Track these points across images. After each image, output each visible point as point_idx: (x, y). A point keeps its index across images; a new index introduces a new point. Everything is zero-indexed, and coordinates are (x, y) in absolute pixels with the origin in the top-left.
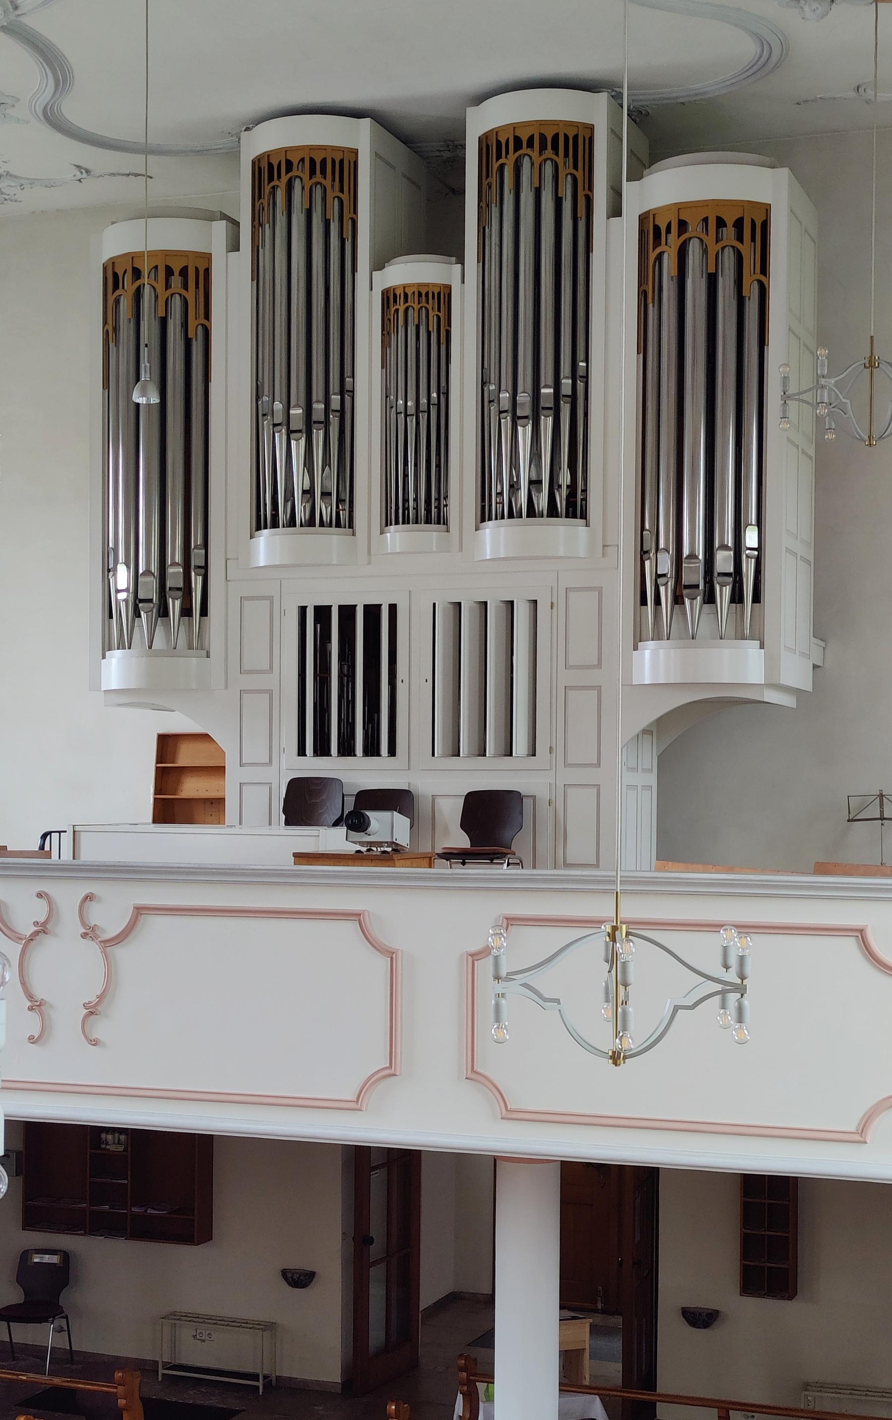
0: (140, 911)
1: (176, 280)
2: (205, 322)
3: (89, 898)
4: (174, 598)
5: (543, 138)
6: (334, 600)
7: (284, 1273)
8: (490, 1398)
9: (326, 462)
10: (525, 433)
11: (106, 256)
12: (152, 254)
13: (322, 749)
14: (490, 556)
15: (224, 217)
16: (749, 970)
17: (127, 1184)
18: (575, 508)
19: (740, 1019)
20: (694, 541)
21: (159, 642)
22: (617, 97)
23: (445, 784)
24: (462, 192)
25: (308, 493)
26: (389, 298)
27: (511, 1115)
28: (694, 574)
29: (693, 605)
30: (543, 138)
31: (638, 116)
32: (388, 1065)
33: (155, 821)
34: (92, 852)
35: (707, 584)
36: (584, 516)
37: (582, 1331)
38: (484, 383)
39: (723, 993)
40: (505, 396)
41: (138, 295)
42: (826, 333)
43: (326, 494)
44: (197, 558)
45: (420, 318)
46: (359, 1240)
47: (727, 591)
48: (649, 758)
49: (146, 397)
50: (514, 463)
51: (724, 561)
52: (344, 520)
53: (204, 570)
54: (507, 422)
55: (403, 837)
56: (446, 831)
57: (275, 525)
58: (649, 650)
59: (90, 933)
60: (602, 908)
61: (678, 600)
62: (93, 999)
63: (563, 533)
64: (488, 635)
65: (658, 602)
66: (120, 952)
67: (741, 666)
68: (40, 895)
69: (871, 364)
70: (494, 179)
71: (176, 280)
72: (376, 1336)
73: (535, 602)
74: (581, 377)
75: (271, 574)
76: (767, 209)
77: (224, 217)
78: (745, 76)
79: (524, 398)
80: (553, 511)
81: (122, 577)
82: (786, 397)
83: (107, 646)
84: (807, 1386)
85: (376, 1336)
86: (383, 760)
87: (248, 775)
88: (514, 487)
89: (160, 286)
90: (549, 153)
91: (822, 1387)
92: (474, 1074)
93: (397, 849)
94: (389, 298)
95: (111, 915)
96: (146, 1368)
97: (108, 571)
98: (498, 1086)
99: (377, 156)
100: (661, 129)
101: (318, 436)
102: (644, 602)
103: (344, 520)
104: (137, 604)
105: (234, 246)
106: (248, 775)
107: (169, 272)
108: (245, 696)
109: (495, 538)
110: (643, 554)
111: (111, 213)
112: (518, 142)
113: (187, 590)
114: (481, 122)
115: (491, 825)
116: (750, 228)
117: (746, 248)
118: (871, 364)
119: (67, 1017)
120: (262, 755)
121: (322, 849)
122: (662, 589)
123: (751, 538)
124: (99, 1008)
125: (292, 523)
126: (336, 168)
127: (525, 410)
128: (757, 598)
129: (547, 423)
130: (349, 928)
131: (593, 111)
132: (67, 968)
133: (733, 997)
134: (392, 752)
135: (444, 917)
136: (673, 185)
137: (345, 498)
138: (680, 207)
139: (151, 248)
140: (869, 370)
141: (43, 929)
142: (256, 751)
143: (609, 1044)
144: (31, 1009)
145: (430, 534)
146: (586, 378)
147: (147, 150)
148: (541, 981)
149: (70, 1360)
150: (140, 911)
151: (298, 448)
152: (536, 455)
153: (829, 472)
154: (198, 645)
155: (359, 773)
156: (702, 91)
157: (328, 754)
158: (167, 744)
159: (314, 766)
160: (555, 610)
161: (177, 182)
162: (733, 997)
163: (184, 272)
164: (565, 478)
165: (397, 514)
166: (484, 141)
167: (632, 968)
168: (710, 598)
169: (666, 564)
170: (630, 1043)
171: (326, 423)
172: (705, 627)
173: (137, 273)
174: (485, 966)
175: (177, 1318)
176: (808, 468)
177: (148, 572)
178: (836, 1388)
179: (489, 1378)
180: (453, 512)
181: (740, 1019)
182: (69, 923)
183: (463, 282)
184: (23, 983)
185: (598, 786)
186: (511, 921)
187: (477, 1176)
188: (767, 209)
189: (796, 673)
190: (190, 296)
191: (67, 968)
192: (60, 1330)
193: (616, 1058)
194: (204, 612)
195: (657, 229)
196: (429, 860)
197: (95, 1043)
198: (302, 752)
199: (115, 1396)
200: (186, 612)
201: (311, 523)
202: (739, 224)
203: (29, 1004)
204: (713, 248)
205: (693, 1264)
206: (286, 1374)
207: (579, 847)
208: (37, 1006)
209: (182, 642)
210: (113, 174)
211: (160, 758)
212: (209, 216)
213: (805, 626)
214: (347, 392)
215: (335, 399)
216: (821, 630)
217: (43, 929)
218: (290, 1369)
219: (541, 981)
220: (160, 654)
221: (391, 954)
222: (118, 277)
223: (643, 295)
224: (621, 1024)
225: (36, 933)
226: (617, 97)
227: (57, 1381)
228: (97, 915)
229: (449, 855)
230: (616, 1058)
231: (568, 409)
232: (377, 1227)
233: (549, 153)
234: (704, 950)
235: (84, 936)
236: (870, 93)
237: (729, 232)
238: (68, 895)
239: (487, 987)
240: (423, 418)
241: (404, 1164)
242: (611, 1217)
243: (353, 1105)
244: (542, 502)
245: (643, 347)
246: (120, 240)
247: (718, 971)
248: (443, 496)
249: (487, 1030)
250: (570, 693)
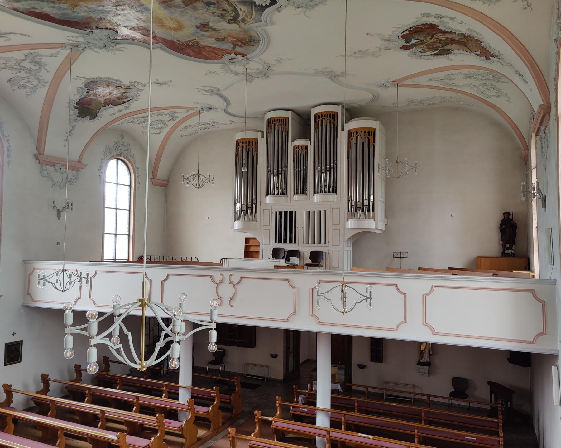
0: (242, 278)
1: (251, 144)
4: (249, 210)
5: (327, 115)
6: (283, 210)
7: (271, 355)
8: (316, 384)
9: (282, 181)
10: (323, 176)
11: (237, 139)
12: (246, 139)
13: (280, 242)
15: (261, 131)
16: (372, 294)
18: (334, 191)
19: (370, 305)
20: (359, 198)
21: (246, 219)
22: (343, 106)
23: (306, 249)
24: (310, 125)
25: (278, 188)
26: (295, 147)
27: (320, 323)
28: (359, 205)
29: (359, 212)
30: (327, 115)
31: (348, 110)
33: (245, 257)
34: (232, 264)
35: (363, 208)
36: (336, 193)
37: (336, 370)
38: (315, 165)
39: (366, 299)
40: (319, 168)
41: (243, 147)
42: (387, 155)
43: (281, 188)
44: (254, 202)
45: (301, 152)
46: (287, 348)
47: (367, 209)
48: (350, 244)
49: (244, 170)
50: (321, 182)
51: (366, 202)
52: (285, 194)
53: (256, 204)
55: (297, 263)
56: (307, 260)
57: (271, 194)
58: (350, 221)
59: (231, 282)
60: (340, 279)
61: (356, 211)
63: (331, 197)
64: (315, 218)
65: (352, 211)
66: (237, 287)
67: (370, 225)
69: (397, 162)
70: (317, 123)
71: (251, 144)
72: (291, 368)
74: (335, 164)
75: (270, 205)
76: (375, 129)
77: (261, 131)
79: (323, 168)
80: (329, 192)
81: (239, 205)
82: (379, 169)
83: (235, 220)
84: (385, 382)
85: (291, 368)
86: (293, 244)
87: (264, 247)
88: (321, 187)
89: (247, 145)
90: (329, 118)
91: (389, 382)
92: (313, 315)
93: (296, 265)
94: (295, 147)
95: (235, 279)
96: (241, 375)
97: (236, 204)
99: (293, 118)
100: (353, 113)
101: (280, 176)
102: (349, 211)
103: (285, 194)
104: (242, 211)
105: (263, 137)
106: (264, 247)
107: (249, 142)
110: (349, 201)
111: (237, 130)
112: (322, 116)
113: (252, 208)
114: (315, 111)
115: (316, 258)
116: (371, 133)
117: (370, 137)
118: (397, 162)
119: (226, 301)
120: (267, 243)
121: (280, 265)
123: (372, 198)
125: (274, 194)
126: (284, 121)
127: (323, 171)
128: (373, 210)
129: (328, 173)
130: (286, 282)
131: (338, 109)
132: (226, 290)
133: (369, 300)
134: (295, 242)
135: (305, 280)
136: (354, 124)
137: (286, 189)
138: (356, 129)
139: (247, 137)
141: (221, 281)
142: (266, 241)
143: (342, 310)
145: (303, 197)
146: (336, 164)
147: (245, 117)
148: (328, 296)
149: (225, 373)
151: (276, 178)
152: (326, 180)
153: (388, 184)
154: (254, 219)
155: (288, 247)
157: (281, 242)
158: (247, 240)
159: (278, 245)
161: (251, 124)
162: (369, 300)
163: (252, 142)
164: (332, 185)
165: (296, 192)
166: (315, 115)
167: (347, 294)
168: (363, 210)
169: (353, 203)
170: (346, 310)
171: (282, 173)
172: (362, 216)
173: (243, 143)
174: (315, 291)
175: (248, 364)
176: (384, 183)
177: (244, 204)
178: (392, 383)
179: (316, 380)
180: (308, 192)
181: (370, 305)
182: (227, 281)
183: (311, 145)
185: (340, 252)
186: (321, 281)
187: (313, 337)
188: (375, 129)
189: (382, 226)
190: (254, 147)
191: (226, 290)
192: (222, 366)
193: (343, 313)
194: (256, 213)
195: (351, 133)
196: (303, 268)
197: (232, 306)
198: (276, 242)
199: (234, 382)
200: (252, 212)
201: (278, 194)
202: (369, 132)
204: (363, 137)
205: (360, 355)
206: (271, 377)
207: (335, 264)
208: (220, 298)
209: (251, 219)
211: (246, 243)
212: (258, 131)
213: (384, 216)
214: (286, 167)
215: (284, 168)
216: (387, 217)
218: (272, 376)
219: (328, 296)
220: (246, 221)
221: (295, 288)
222: (239, 143)
223: (348, 147)
224: (344, 306)
226: (343, 106)
227: (222, 378)
228: (233, 279)
229: (307, 265)
230: (343, 313)
231: (333, 170)
232: (291, 345)
233: (329, 118)
234: (362, 289)
236: (396, 105)
237: (367, 134)
238: (227, 274)
239: (316, 297)
241: (297, 333)
242: (342, 345)
244: (327, 190)
245: (348, 158)
246: (239, 136)
247: (365, 294)
248: (306, 188)
249: (316, 307)
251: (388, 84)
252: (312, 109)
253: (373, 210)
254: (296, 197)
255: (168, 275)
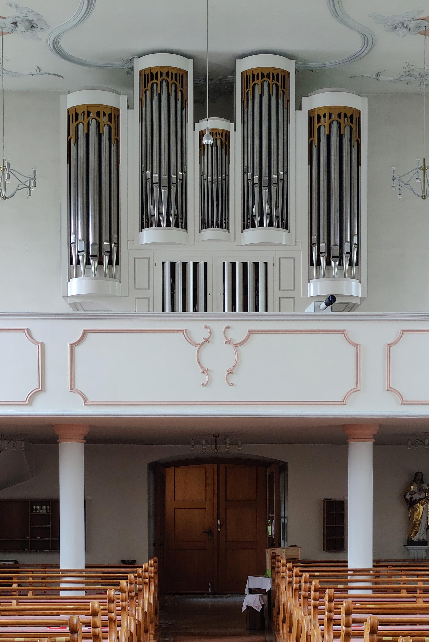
0: (251, 332)
2: (117, 138)
3: (228, 328)
5: (262, 74)
14: (248, 243)
17: (49, 527)
18: (284, 224)
27: (405, 403)
29: (334, 265)
32: (356, 387)
51: (347, 249)
52: (181, 223)
53: (117, 244)
54: (257, 189)
58: (74, 281)
61: (328, 263)
62: (231, 367)
63: (277, 235)
65: (319, 264)
66: (241, 349)
68: (206, 327)
73: (267, 263)
78: (346, 61)
94: (315, 117)
98: (400, 393)
103: (181, 223)
108: (137, 300)
109: (253, 235)
122: (322, 258)
124: (233, 371)
126: (179, 77)
127: (165, 182)
128: (357, 264)
130: (340, 336)
131: (290, 66)
140: (423, 171)
141: (207, 341)
144: (203, 372)
150: (251, 332)
156: (325, 65)
160: (275, 267)
168: (341, 264)
169: (323, 246)
182: (219, 338)
184: (199, 362)
197: (232, 385)
203: (202, 370)
210: (49, 74)
217: (207, 341)
222: (73, 116)
225: (204, 342)
235: (226, 342)
240: (220, 184)
243: (342, 403)
246: (75, 99)
250: (282, 300)
251: (412, 25)
252: (237, 61)
253: (357, 264)
254: (210, 233)
255: (85, 332)
